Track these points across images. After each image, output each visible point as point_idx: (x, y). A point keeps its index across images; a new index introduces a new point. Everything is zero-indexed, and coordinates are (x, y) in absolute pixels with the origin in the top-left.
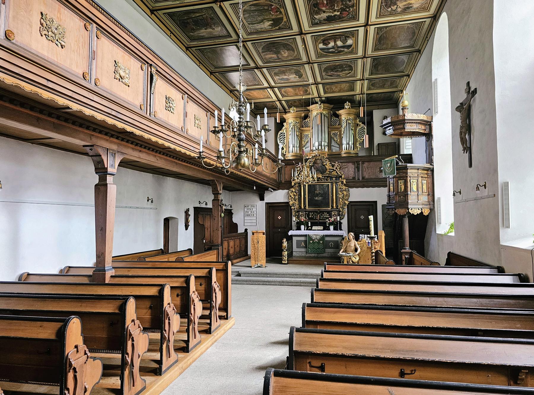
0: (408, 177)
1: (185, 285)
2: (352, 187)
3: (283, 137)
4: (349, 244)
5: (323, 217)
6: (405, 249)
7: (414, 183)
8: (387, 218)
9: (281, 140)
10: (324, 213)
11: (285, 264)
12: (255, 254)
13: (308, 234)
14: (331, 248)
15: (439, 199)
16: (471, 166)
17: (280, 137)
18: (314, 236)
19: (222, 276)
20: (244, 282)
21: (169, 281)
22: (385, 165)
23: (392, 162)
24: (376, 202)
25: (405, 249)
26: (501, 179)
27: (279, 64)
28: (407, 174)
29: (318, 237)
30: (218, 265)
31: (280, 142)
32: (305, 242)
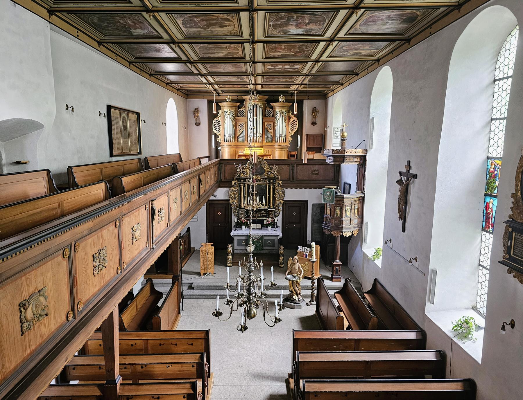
0: (344, 205)
1: (192, 392)
3: (218, 125)
4: (294, 267)
5: (261, 215)
8: (315, 215)
9: (216, 127)
10: (262, 211)
12: (204, 264)
14: (269, 246)
15: (367, 223)
16: (404, 230)
18: (254, 236)
20: (198, 297)
23: (331, 192)
24: (307, 201)
25: (336, 262)
26: (431, 266)
28: (343, 202)
29: (258, 237)
31: (215, 130)
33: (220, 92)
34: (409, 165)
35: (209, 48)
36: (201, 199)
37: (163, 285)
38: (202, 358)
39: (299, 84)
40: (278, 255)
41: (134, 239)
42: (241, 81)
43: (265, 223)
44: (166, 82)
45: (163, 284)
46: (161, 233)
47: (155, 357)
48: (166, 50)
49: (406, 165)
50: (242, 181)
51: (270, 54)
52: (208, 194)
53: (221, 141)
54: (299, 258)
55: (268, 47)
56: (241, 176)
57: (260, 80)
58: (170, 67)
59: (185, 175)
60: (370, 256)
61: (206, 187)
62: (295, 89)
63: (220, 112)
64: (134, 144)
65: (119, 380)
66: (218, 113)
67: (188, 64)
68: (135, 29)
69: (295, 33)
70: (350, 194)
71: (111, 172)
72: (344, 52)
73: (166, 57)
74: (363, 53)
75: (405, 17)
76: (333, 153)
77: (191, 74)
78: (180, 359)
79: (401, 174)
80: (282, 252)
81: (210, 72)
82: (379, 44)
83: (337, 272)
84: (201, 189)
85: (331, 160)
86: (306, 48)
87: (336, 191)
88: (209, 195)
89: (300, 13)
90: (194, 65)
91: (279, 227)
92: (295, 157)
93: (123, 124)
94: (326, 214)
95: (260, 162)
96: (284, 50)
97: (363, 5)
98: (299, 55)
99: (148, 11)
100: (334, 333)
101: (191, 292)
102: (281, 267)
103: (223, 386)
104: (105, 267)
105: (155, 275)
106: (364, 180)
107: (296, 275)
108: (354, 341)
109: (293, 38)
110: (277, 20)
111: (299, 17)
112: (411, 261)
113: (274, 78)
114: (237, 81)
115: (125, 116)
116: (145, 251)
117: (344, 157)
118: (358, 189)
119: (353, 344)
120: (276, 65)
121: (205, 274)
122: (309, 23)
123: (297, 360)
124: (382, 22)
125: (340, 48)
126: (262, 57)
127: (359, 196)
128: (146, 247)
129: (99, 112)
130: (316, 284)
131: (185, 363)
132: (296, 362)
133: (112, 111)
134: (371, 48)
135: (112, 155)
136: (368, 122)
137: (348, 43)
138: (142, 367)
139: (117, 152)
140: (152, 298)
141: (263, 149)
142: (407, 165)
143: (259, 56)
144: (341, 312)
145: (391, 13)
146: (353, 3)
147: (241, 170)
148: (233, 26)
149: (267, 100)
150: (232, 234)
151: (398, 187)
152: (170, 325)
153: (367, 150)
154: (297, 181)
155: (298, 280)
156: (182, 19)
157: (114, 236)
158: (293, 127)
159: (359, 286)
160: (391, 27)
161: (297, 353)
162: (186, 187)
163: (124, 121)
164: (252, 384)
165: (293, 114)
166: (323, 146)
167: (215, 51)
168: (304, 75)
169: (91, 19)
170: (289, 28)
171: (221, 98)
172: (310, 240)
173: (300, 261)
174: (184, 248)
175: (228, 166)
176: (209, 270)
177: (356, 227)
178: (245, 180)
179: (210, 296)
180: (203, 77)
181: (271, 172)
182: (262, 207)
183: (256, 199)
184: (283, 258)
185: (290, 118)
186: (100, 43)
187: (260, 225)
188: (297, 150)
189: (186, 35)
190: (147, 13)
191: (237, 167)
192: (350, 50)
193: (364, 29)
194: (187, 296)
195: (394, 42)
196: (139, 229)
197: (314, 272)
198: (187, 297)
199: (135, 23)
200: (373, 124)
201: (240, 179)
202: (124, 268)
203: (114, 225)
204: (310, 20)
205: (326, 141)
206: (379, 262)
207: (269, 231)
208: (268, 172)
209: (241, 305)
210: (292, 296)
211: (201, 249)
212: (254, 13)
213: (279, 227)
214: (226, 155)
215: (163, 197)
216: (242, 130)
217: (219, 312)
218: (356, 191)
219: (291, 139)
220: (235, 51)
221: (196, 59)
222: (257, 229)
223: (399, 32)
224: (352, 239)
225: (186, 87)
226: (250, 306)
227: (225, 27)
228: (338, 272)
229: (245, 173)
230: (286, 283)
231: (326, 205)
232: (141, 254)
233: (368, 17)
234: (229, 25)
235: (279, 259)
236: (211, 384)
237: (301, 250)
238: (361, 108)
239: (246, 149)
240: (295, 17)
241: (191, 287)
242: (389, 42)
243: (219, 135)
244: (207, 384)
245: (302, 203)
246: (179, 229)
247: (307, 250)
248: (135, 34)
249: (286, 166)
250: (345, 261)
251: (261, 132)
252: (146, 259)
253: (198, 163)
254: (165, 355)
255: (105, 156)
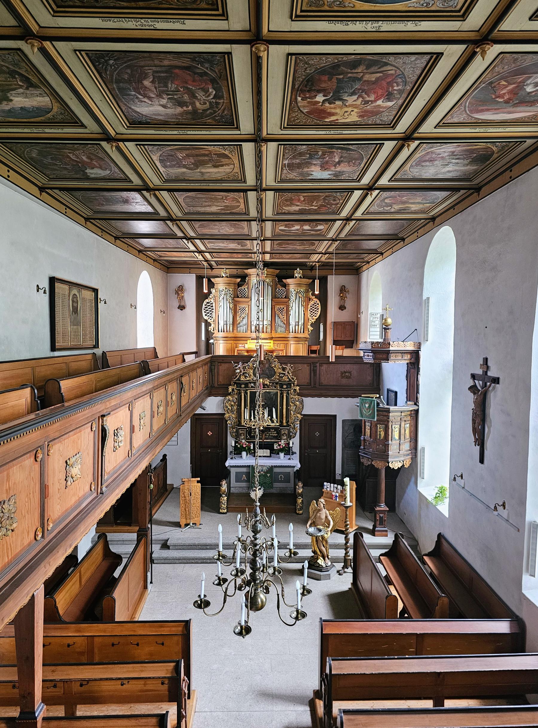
0: (390, 422)
2: (307, 396)
3: (209, 308)
4: (318, 514)
5: (269, 436)
6: (380, 506)
7: (396, 430)
8: (347, 436)
9: (207, 312)
10: (271, 430)
11: (223, 513)
12: (186, 511)
13: (251, 464)
14: (281, 482)
15: (423, 449)
16: (482, 461)
17: (206, 308)
19: (181, 640)
20: (176, 561)
21: (134, 724)
22: (362, 405)
24: (335, 416)
25: (380, 506)
27: (176, 132)
28: (389, 418)
29: (265, 468)
30: (175, 627)
31: (206, 315)
32: (248, 474)
33: (213, 263)
34: (487, 364)
35: (198, 198)
36: (182, 413)
37: (123, 542)
38: (177, 669)
39: (322, 253)
40: (294, 496)
41: (69, 479)
42: (243, 248)
43: (275, 448)
44: (139, 249)
45: (123, 541)
46: (118, 467)
47: (103, 668)
48: (137, 201)
49: (481, 365)
50: (243, 386)
51: (284, 208)
52: (193, 405)
53: (214, 331)
54: (326, 501)
55: (281, 198)
56: (242, 379)
57: (268, 246)
58: (144, 227)
59: (159, 378)
60: (430, 498)
61: (191, 395)
62: (317, 260)
63: (213, 291)
64: (88, 332)
65: (40, 712)
66: (210, 292)
67: (168, 222)
68: (93, 168)
69: (319, 177)
70: (396, 405)
71: (48, 372)
72: (387, 207)
73: (137, 211)
74: (412, 209)
75: (475, 155)
76: (372, 347)
77: (173, 236)
78: (142, 671)
79: (473, 376)
80: (300, 491)
81: (199, 235)
82: (435, 195)
83: (382, 522)
84: (183, 398)
85: (369, 358)
86: (335, 200)
87: (379, 401)
88: (194, 407)
89: (327, 147)
90: (177, 224)
91: (295, 453)
92: (316, 353)
93: (73, 305)
94: (365, 435)
95: (269, 359)
96: (304, 203)
97: (418, 134)
98: (323, 210)
99: (109, 139)
100: (385, 624)
101: (166, 553)
102: (298, 514)
103: (210, 713)
104: (13, 531)
105: (113, 526)
106: (418, 386)
107: (321, 527)
108: (415, 637)
109: (316, 184)
110: (294, 157)
111: (326, 152)
112: (495, 508)
113: (288, 244)
114: (237, 248)
115: (76, 293)
116: (87, 498)
117: (388, 353)
118: (409, 399)
119: (413, 641)
120: (292, 224)
121: (187, 525)
122: (339, 163)
123: (328, 671)
124: (441, 161)
125: (381, 201)
126: (271, 213)
127: (411, 409)
128: (91, 490)
129: (38, 286)
130: (351, 541)
131: (150, 678)
132: (326, 674)
133: (57, 285)
134: (425, 202)
135: (53, 348)
136: (421, 304)
137: (393, 192)
138: (81, 685)
139: (62, 344)
140: (106, 564)
141: (272, 341)
142: (483, 364)
143: (269, 212)
144: (391, 584)
145: (456, 148)
146: (477, 29)
147: (241, 371)
148: (232, 166)
149: (277, 276)
150: (227, 464)
151: (471, 397)
152: (130, 609)
153: (420, 343)
154: (320, 387)
155: (326, 535)
156: (158, 155)
157: (32, 476)
158: (314, 311)
159: (414, 543)
160: (454, 169)
161: (327, 660)
162: (159, 395)
163: (75, 300)
164: (257, 709)
165: (313, 294)
166: (355, 339)
167: (207, 204)
168: (329, 240)
169: (27, 152)
170: (311, 170)
171: (215, 272)
172: (340, 473)
173: (330, 506)
174: (157, 486)
175: (223, 365)
176: (194, 518)
177: (408, 455)
178: (246, 385)
179: (193, 559)
180: (189, 241)
181: (284, 374)
182: (271, 424)
183: (264, 413)
184: (302, 500)
185: (310, 300)
186: (42, 189)
187: (269, 451)
188: (319, 343)
189: (166, 178)
190: (108, 143)
191: (236, 366)
192: (395, 204)
193: (416, 172)
194: (160, 559)
195: (457, 191)
196: (79, 462)
197: (348, 523)
198: (159, 561)
199: (92, 160)
200: (428, 306)
201: (241, 384)
202: (49, 529)
203: (34, 457)
204: (341, 157)
205: (359, 333)
206: (444, 508)
207: (281, 460)
208: (280, 374)
209: (240, 589)
210: (316, 560)
211: (181, 487)
212: (263, 144)
213: (295, 453)
214: (220, 349)
215: (122, 411)
216: (243, 316)
217: (205, 600)
218: (406, 402)
219: (311, 328)
220: (234, 204)
221: (179, 214)
222: (264, 456)
223: (465, 177)
224: (401, 472)
225: (166, 256)
226: (255, 590)
227: (220, 168)
228: (383, 522)
229: (247, 375)
230: (308, 540)
231: (363, 422)
232: (80, 502)
233: (423, 153)
234: (226, 164)
235: (296, 502)
236: (191, 711)
237: (328, 489)
238: (410, 285)
239: (248, 341)
240: (320, 153)
241: (165, 546)
242: (451, 192)
243: (211, 323)
244: (186, 713)
245: (329, 418)
246: (147, 459)
247: (337, 488)
248: (93, 176)
249: (306, 366)
250: (392, 504)
251: (269, 318)
252: (88, 512)
253: (181, 360)
254: (119, 665)
255: (44, 350)
